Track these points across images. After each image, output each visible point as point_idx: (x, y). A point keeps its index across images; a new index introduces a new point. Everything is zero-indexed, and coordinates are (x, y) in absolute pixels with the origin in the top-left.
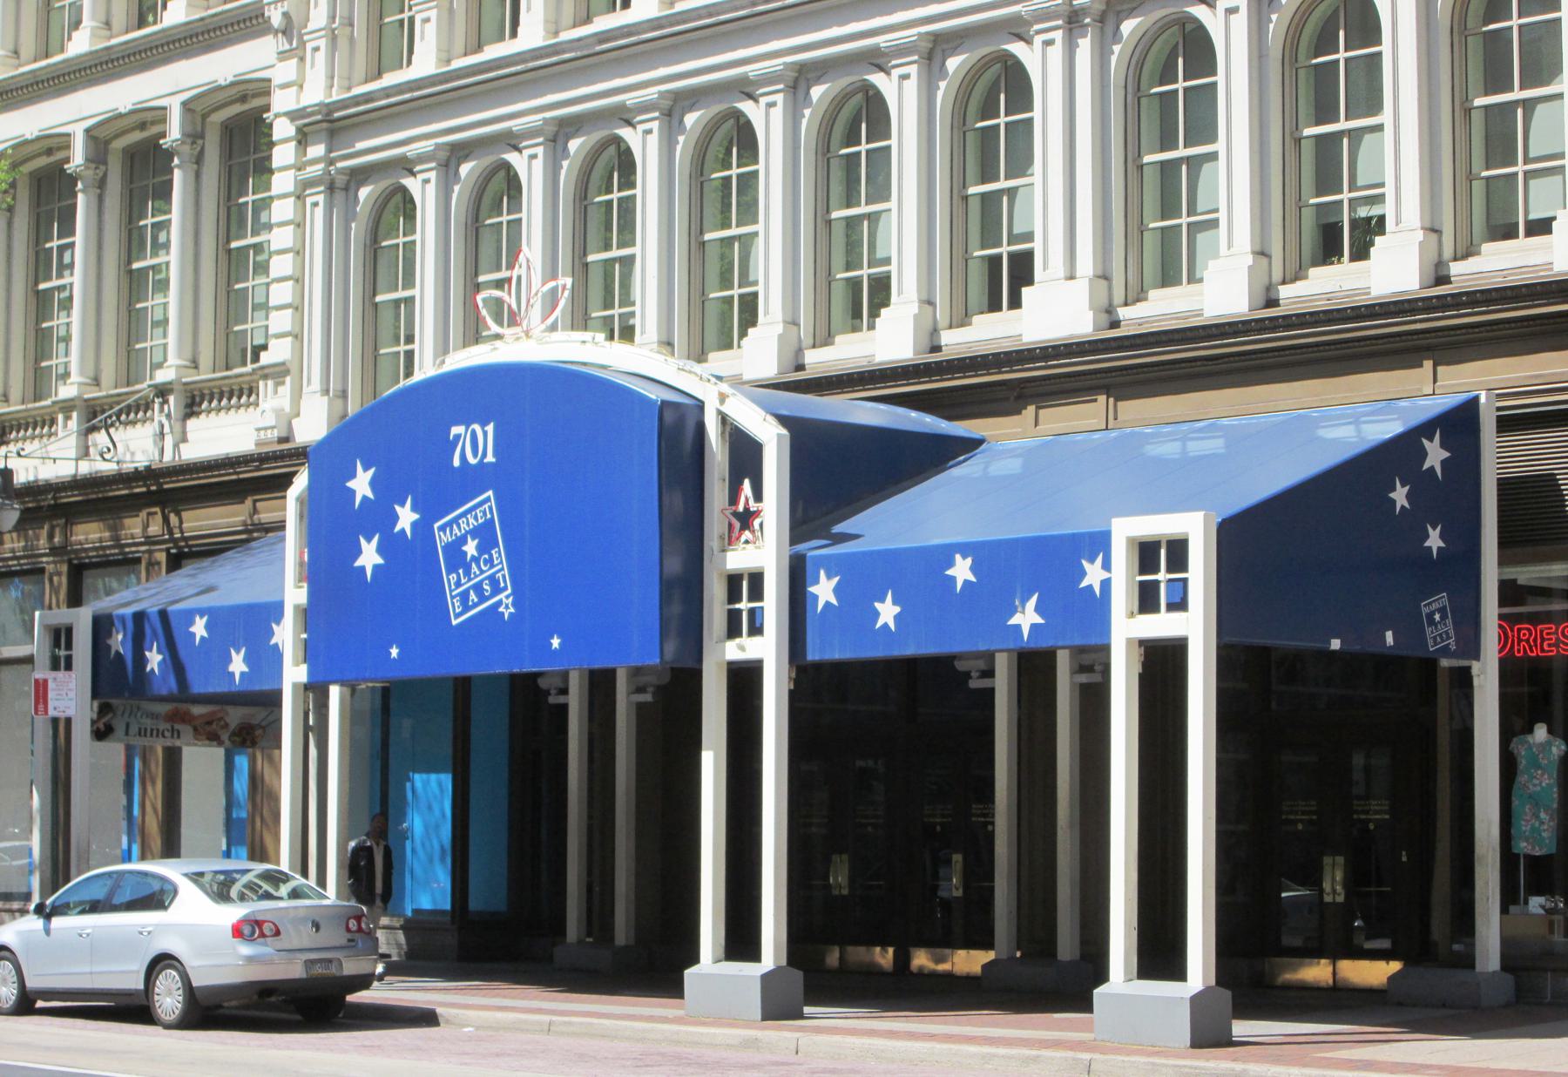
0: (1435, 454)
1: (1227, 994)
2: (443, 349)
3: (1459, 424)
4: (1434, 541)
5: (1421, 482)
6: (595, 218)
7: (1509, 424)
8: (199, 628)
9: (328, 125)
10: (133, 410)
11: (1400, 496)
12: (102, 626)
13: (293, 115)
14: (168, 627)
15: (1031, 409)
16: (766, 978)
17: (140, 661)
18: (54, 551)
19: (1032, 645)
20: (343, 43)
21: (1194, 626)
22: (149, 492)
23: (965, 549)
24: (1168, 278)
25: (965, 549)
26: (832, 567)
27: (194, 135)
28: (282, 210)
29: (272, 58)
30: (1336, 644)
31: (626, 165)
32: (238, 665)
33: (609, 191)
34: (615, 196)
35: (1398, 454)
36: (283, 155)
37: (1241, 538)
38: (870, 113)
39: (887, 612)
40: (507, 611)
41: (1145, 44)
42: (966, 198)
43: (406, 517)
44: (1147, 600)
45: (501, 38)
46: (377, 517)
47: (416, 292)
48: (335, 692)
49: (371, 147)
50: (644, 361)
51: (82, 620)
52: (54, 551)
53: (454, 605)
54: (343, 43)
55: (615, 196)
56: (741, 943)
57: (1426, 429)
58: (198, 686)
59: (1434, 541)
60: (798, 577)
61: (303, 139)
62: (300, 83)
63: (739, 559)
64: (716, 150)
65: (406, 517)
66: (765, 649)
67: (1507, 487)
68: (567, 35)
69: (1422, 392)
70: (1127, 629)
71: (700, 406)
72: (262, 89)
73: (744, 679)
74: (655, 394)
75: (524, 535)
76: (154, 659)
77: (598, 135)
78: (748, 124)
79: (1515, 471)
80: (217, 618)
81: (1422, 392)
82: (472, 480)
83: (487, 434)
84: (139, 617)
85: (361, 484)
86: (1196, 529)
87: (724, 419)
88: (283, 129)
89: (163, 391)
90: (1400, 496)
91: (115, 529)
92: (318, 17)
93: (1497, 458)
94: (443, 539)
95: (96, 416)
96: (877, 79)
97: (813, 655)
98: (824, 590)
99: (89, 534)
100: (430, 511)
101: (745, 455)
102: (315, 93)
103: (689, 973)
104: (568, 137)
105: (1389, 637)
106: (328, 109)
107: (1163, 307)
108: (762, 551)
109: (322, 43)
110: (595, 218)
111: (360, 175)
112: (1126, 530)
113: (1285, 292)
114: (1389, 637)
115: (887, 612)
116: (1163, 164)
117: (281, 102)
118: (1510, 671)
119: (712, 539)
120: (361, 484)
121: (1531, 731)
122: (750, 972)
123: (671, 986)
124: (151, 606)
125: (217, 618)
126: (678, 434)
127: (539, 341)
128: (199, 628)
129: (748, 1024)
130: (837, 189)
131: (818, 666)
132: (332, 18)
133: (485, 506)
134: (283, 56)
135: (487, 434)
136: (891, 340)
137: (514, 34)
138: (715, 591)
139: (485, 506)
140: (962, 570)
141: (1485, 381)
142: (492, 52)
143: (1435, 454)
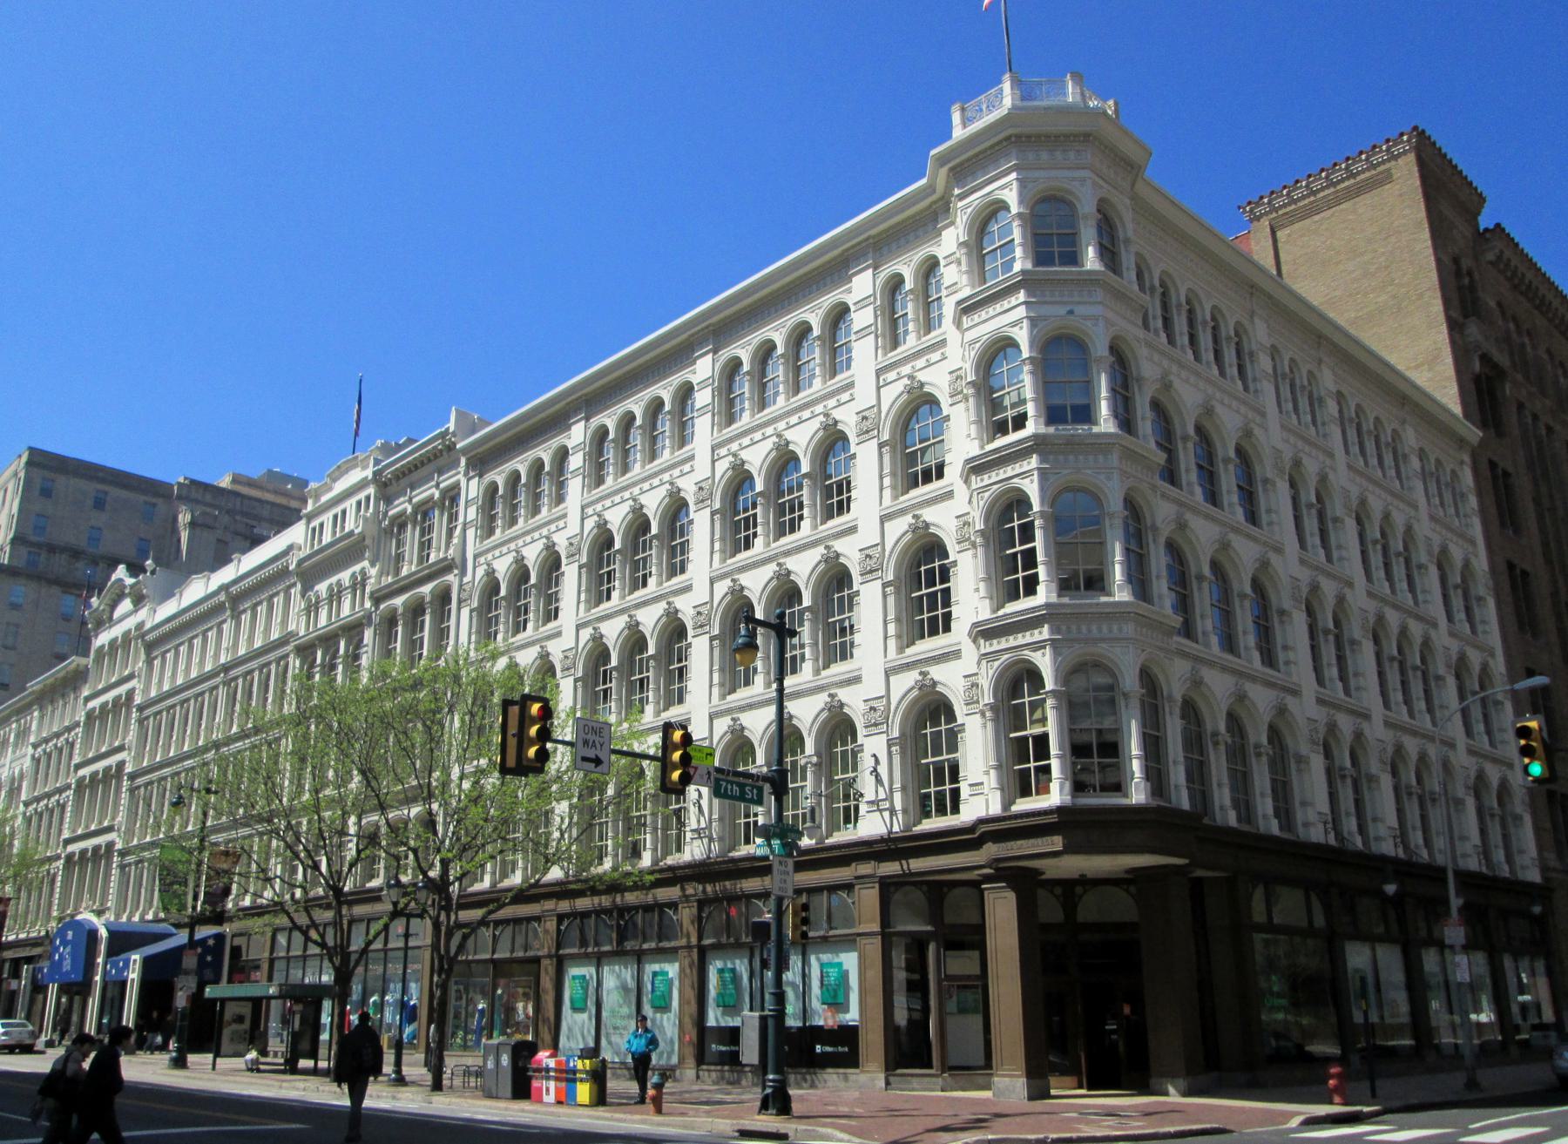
4: (209, 958)
66: (98, 978)
126: (92, 934)
133: (68, 949)
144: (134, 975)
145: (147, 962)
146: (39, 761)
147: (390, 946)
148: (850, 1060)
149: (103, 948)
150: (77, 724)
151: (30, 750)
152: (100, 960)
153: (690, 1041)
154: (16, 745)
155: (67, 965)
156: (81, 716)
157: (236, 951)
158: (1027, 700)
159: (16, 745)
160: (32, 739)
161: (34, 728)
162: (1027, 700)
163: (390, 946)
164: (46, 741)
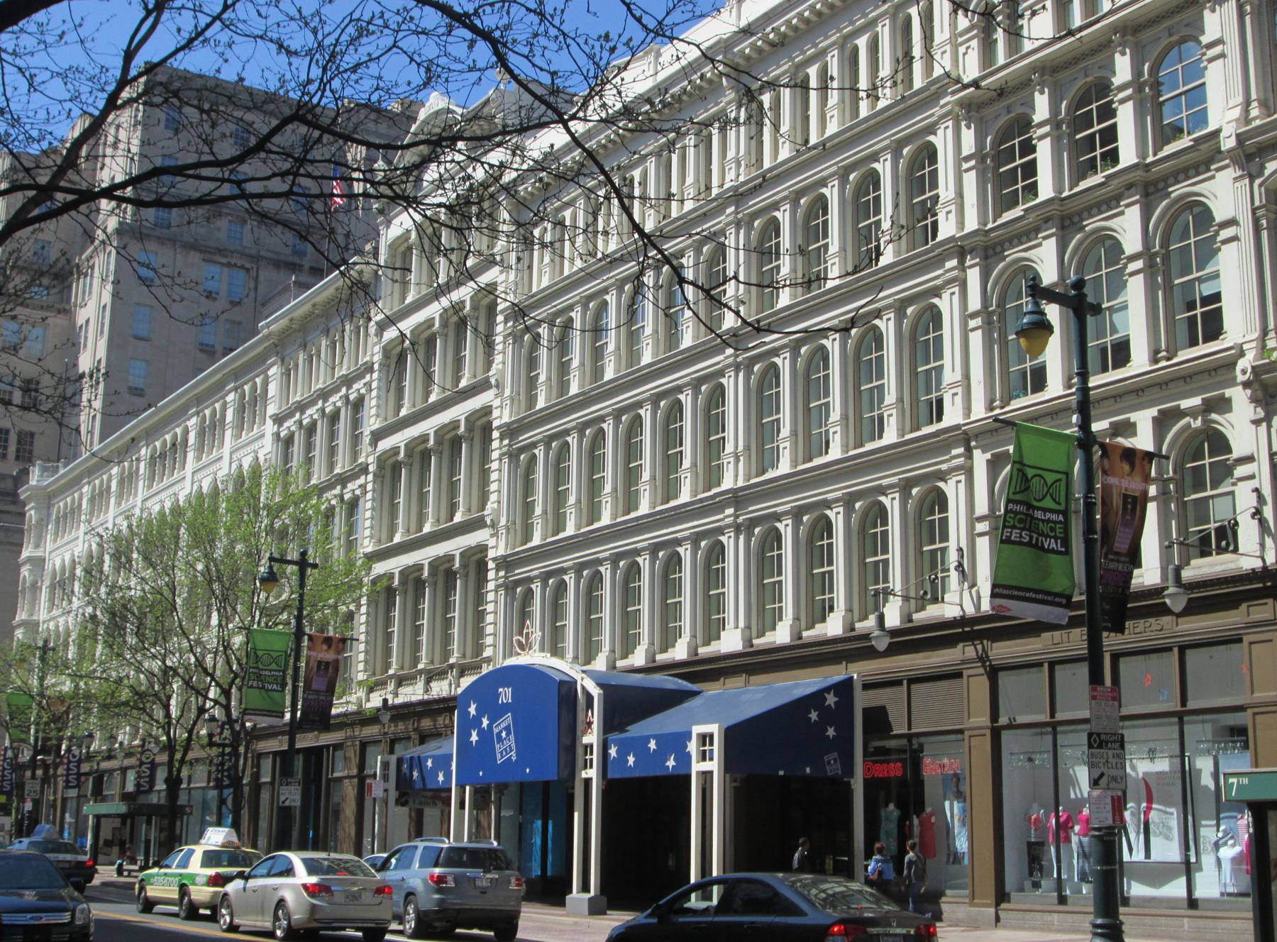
0: (831, 699)
1: (605, 899)
2: (504, 658)
3: (844, 689)
4: (831, 732)
5: (824, 710)
6: (816, 553)
7: (866, 687)
8: (429, 763)
9: (506, 563)
10: (441, 674)
11: (814, 716)
12: (400, 761)
13: (494, 559)
14: (418, 762)
15: (961, 645)
16: (590, 899)
17: (412, 776)
18: (415, 730)
19: (676, 773)
20: (512, 531)
21: (714, 766)
22: (1265, 588)
23: (655, 737)
24: (935, 600)
25: (655, 737)
26: (617, 743)
27: (464, 565)
28: (491, 597)
29: (488, 536)
30: (781, 773)
31: (829, 527)
32: (441, 778)
33: (822, 539)
34: (879, 530)
35: (816, 699)
36: (491, 575)
37: (733, 735)
38: (826, 527)
39: (631, 760)
40: (514, 759)
41: (922, 499)
42: (813, 575)
43: (485, 722)
44: (703, 757)
45: (821, 455)
46: (476, 722)
47: (834, 568)
48: (468, 788)
49: (757, 509)
50: (564, 666)
51: (393, 759)
52: (415, 730)
53: (499, 756)
54: (512, 531)
55: (879, 530)
56: (585, 887)
57: (827, 690)
58: (429, 786)
59: (831, 732)
60: (605, 747)
61: (498, 569)
62: (498, 548)
63: (586, 740)
64: (817, 534)
65: (485, 722)
66: (592, 773)
67: (866, 711)
68: (658, 508)
69: (836, 674)
70: (697, 767)
71: (576, 682)
72: (483, 549)
73: (588, 782)
74: (558, 677)
75: (519, 729)
76: (415, 774)
77: (816, 514)
78: (885, 507)
79: (867, 705)
80: (435, 759)
81: (836, 674)
82: (505, 708)
83: (509, 691)
84: (412, 758)
85: (472, 710)
86: (714, 728)
87: (583, 688)
88: (491, 565)
89: (452, 667)
90: (814, 716)
91: (435, 721)
92: (503, 521)
93: (862, 700)
94: (496, 731)
95: (431, 676)
96: (882, 499)
97: (610, 776)
98: (613, 752)
99: (426, 723)
100: (492, 721)
101: (589, 698)
102: (501, 551)
103: (568, 897)
104: (912, 487)
105: (808, 770)
106: (505, 557)
107: (932, 612)
108: (592, 738)
109: (732, 460)
110: (816, 553)
111: (518, 583)
112: (697, 730)
113: (805, 634)
114: (808, 770)
115: (631, 760)
116: (931, 551)
117: (491, 554)
118: (868, 783)
119: (579, 733)
120: (472, 710)
121: (887, 806)
122: (587, 896)
123: (562, 904)
124: (416, 755)
125: (435, 759)
126: (567, 691)
127: (536, 658)
128: (429, 763)
129: (582, 916)
130: (925, 537)
131: (612, 780)
132: (736, 447)
133: (508, 719)
134: (492, 535)
135: (509, 691)
136: (680, 652)
137: (827, 453)
138: (580, 751)
139: (508, 719)
140: (652, 745)
141: (857, 671)
142: (818, 461)
143: (831, 699)
144: (707, 766)
145: (740, 740)
146: (289, 441)
147: (1059, 716)
148: (113, 800)
149: (596, 716)
150: (369, 368)
151: (270, 427)
152: (592, 738)
153: (1236, 861)
154: (120, 496)
155: (506, 750)
156: (374, 354)
157: (877, 720)
158: (1207, 461)
159: (120, 496)
160: (272, 409)
161: (273, 389)
162: (1207, 461)
163: (1059, 716)
164: (302, 407)
